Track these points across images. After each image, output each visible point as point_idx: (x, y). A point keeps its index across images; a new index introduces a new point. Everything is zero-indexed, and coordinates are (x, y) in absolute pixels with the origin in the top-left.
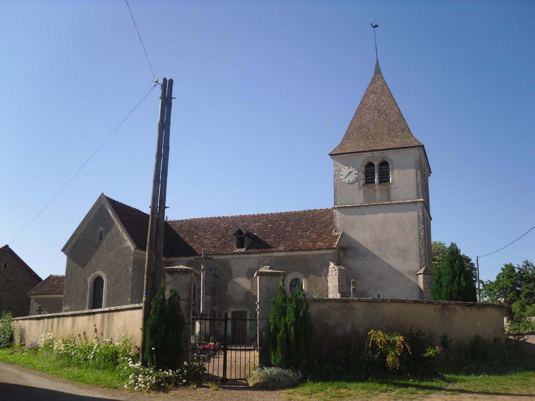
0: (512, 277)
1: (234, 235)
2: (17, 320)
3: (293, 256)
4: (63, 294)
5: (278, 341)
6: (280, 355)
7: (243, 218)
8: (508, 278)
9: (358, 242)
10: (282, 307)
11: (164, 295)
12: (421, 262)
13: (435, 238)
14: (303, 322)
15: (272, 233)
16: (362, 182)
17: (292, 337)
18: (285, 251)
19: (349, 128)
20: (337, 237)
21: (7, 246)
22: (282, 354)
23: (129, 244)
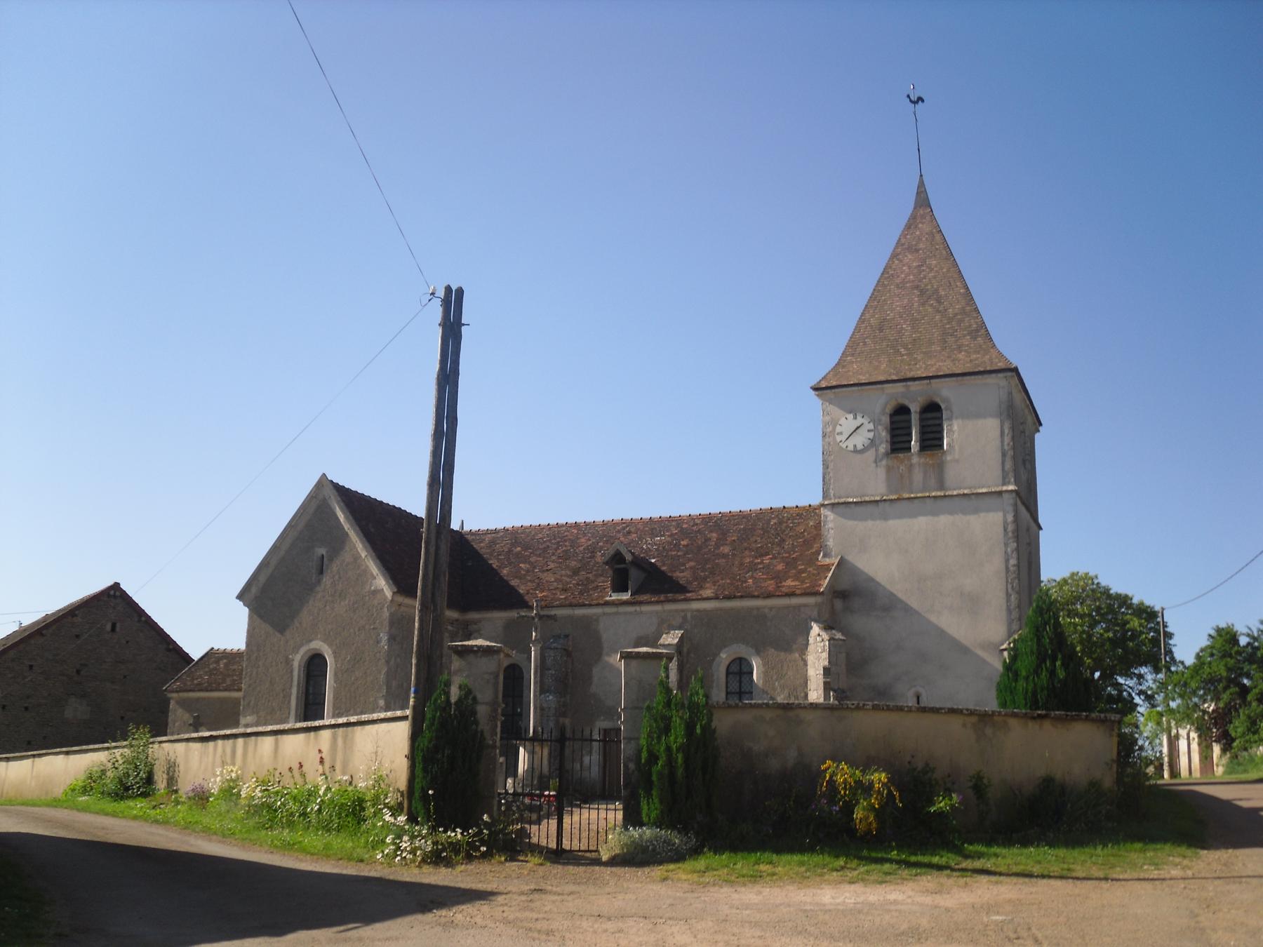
0: (1230, 656)
1: (606, 563)
2: (160, 742)
3: (732, 609)
4: (240, 690)
5: (654, 778)
6: (657, 805)
7: (627, 526)
8: (1223, 656)
9: (872, 580)
10: (664, 718)
11: (447, 694)
12: (1010, 624)
13: (1055, 566)
14: (702, 746)
15: (690, 560)
16: (883, 448)
17: (680, 772)
18: (716, 598)
19: (857, 329)
20: (827, 568)
21: (117, 585)
22: (661, 802)
23: (382, 583)
